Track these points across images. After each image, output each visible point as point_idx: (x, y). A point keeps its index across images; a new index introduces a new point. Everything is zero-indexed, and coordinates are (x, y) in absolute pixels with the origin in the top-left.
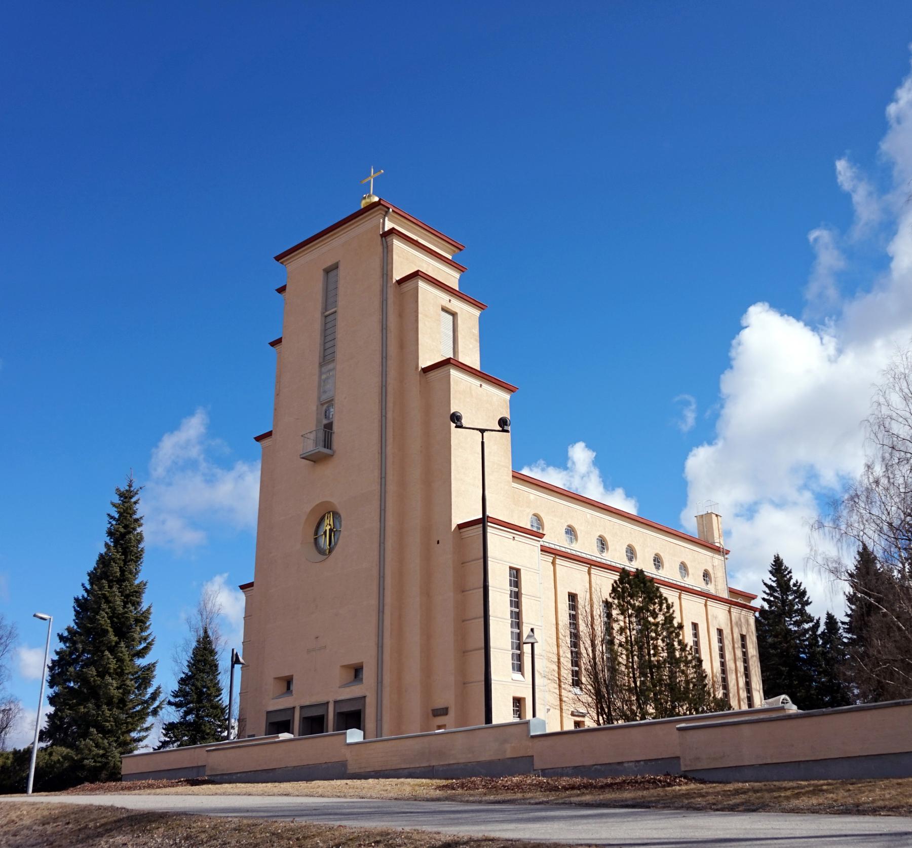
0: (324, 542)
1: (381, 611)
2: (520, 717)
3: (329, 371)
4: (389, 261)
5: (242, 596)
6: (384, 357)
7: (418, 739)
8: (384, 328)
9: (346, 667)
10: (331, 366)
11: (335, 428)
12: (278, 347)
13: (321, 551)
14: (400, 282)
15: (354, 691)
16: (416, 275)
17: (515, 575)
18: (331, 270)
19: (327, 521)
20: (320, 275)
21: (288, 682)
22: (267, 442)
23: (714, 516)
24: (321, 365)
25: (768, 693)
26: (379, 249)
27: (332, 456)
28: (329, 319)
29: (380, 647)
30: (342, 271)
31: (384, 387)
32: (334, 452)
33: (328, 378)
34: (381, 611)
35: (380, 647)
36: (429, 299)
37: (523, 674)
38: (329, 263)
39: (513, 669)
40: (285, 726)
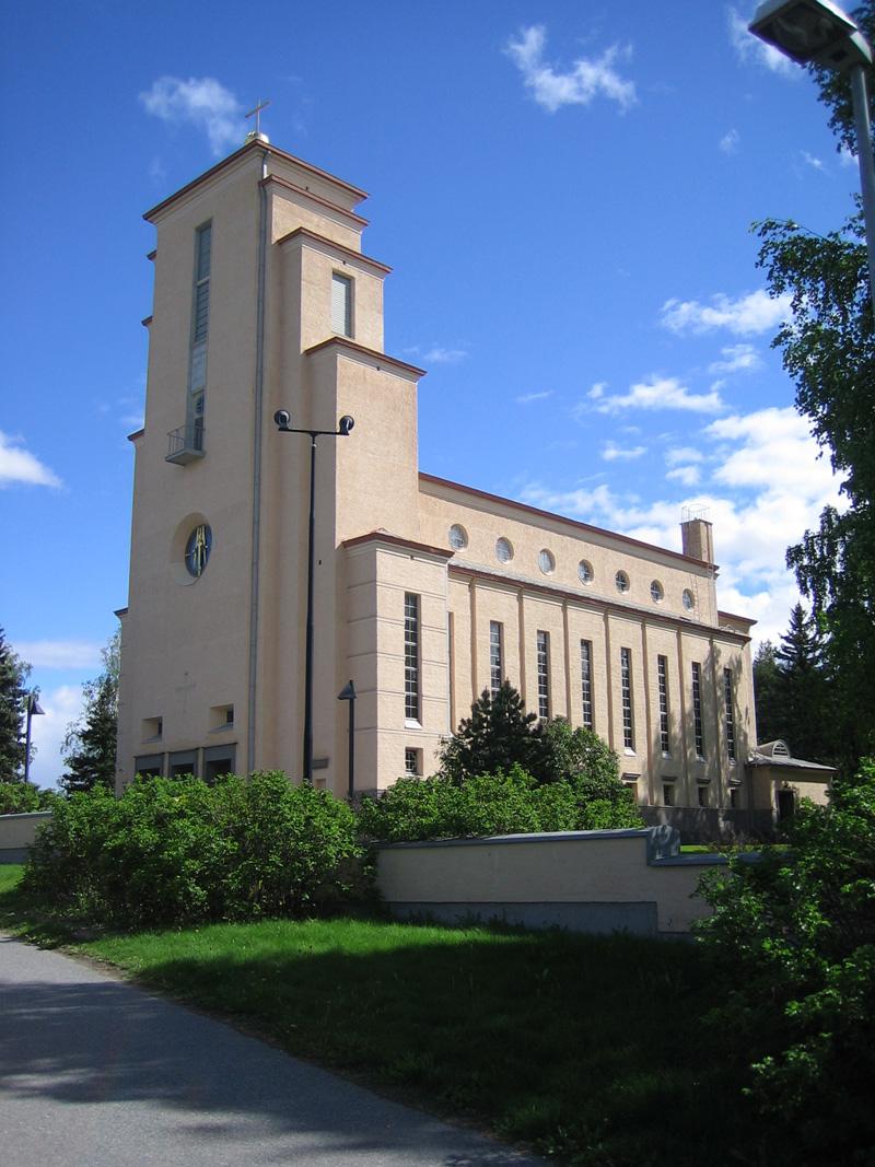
0: (196, 560)
1: (253, 646)
2: (414, 771)
3: (201, 354)
4: (268, 232)
5: (117, 621)
6: (261, 336)
7: (331, 172)
8: (261, 301)
9: (218, 709)
10: (203, 348)
11: (206, 425)
12: (150, 326)
13: (193, 573)
14: (281, 242)
15: (225, 738)
16: (299, 232)
17: (413, 600)
18: (204, 230)
19: (198, 537)
20: (192, 236)
21: (158, 724)
22: (140, 440)
23: (702, 524)
24: (192, 348)
25: (764, 735)
26: (256, 200)
27: (203, 457)
28: (203, 290)
29: (253, 686)
30: (216, 230)
31: (259, 372)
32: (205, 453)
33: (199, 363)
34: (253, 646)
35: (253, 686)
36: (315, 266)
37: (420, 721)
38: (199, 222)
39: (408, 715)
40: (156, 772)
